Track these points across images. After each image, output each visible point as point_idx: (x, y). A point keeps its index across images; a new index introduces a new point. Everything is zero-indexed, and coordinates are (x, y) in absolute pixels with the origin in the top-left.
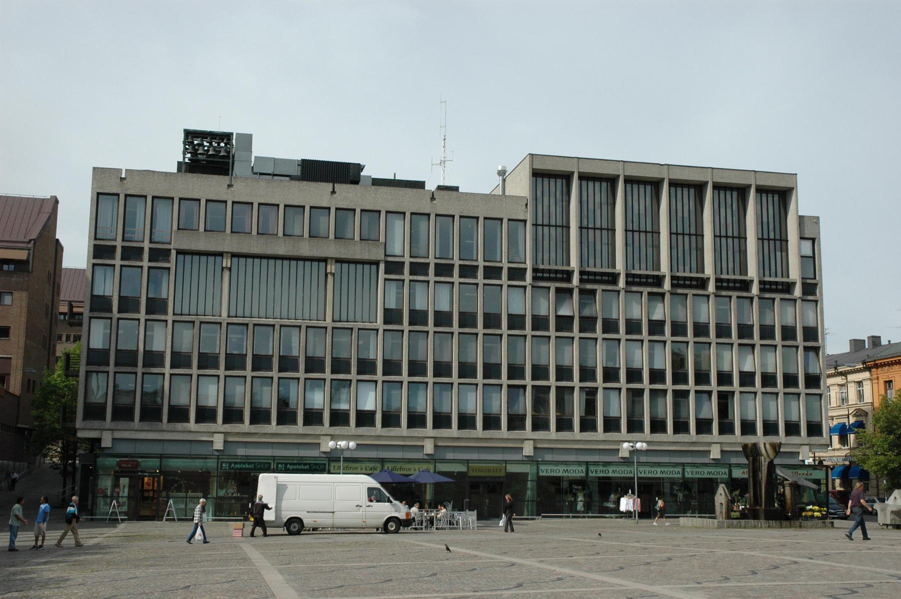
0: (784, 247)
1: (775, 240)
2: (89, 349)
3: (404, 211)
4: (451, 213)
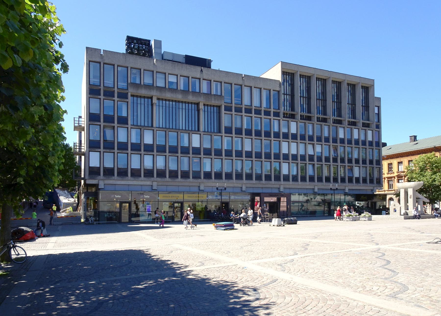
0: (368, 110)
1: (305, 97)
2: (144, 144)
3: (140, 68)
4: (113, 63)
